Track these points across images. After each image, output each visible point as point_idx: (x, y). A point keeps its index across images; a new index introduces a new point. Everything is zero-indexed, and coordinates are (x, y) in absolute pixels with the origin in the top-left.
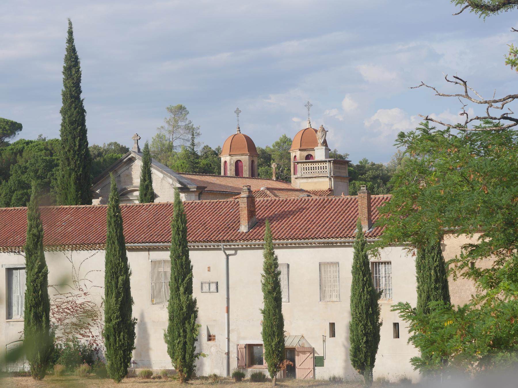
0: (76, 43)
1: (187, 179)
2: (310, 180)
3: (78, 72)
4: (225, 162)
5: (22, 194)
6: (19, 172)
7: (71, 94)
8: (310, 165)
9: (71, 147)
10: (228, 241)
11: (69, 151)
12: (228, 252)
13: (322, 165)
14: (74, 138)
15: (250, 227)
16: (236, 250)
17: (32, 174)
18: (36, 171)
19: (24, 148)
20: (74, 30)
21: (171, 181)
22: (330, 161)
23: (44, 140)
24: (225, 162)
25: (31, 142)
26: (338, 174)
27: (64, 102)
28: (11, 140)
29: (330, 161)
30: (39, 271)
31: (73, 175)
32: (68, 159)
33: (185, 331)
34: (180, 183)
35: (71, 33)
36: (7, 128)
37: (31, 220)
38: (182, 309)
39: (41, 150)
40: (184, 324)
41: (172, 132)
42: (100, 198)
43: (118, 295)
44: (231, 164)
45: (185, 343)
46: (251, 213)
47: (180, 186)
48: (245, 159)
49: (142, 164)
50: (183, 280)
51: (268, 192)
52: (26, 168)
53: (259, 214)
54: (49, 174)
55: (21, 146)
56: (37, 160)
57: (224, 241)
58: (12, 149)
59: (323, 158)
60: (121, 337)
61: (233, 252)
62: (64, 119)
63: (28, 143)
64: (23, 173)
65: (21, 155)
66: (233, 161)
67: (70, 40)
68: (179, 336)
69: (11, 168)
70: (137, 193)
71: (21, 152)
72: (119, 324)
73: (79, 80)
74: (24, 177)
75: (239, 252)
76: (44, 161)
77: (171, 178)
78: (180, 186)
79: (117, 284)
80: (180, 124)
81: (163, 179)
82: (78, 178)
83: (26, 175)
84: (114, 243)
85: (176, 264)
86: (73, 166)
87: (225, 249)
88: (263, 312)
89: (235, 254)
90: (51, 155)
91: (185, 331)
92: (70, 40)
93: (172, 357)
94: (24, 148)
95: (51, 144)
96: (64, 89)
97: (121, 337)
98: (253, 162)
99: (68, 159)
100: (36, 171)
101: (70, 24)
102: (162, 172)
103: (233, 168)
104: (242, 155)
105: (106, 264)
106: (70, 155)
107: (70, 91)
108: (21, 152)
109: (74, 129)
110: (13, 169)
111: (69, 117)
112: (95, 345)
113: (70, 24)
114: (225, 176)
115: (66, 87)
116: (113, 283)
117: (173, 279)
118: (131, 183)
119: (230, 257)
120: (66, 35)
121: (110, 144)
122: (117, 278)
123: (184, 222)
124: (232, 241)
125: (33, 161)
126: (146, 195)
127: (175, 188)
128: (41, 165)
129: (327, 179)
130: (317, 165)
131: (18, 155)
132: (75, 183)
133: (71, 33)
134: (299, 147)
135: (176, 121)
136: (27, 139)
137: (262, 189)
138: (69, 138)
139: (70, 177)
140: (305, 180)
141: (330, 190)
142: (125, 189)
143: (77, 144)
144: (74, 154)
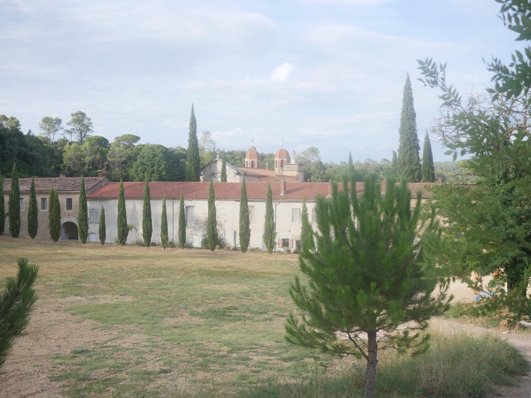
0: (195, 113)
1: (239, 170)
2: (289, 172)
3: (196, 125)
4: (247, 161)
5: (143, 168)
6: (141, 158)
7: (193, 134)
8: (289, 166)
9: (192, 155)
10: (276, 199)
11: (192, 157)
12: (276, 203)
13: (294, 166)
14: (194, 152)
15: (285, 194)
16: (279, 202)
17: (147, 159)
18: (148, 158)
19: (142, 147)
20: (194, 108)
21: (233, 170)
22: (297, 164)
23: (149, 144)
24: (247, 161)
25: (145, 145)
26: (300, 170)
27: (190, 137)
28: (135, 144)
29: (297, 164)
30: (214, 210)
31: (193, 167)
32: (191, 160)
33: (271, 235)
34: (237, 171)
35: (193, 109)
36: (135, 139)
37: (210, 191)
38: (270, 226)
39: (150, 149)
40: (271, 232)
41: (204, 143)
42: (203, 176)
43: (245, 220)
44: (250, 162)
45: (271, 239)
46: (285, 188)
47: (236, 172)
48: (256, 161)
49: (222, 163)
50: (271, 215)
51: (277, 177)
52: (144, 157)
53: (288, 189)
54: (154, 159)
55: (140, 147)
56: (148, 153)
57: (275, 199)
58: (137, 148)
59: (294, 163)
60: (246, 236)
61: (278, 203)
62: (190, 144)
63: (143, 146)
64: (143, 158)
65: (141, 151)
66: (251, 162)
67: (193, 112)
68: (269, 236)
69: (137, 156)
70: (220, 175)
71: (141, 149)
72: (245, 231)
73: (196, 128)
74: (143, 160)
75: (281, 203)
76: (152, 154)
77: (233, 169)
78: (236, 172)
79: (245, 216)
80: (207, 139)
81: (229, 169)
82: (195, 168)
83: (144, 160)
84: (244, 201)
85: (268, 209)
86: (193, 163)
87: (275, 202)
88: (302, 228)
89: (279, 204)
90: (154, 151)
91: (271, 235)
92: (193, 112)
93: (266, 244)
94: (142, 147)
95: (154, 146)
96: (190, 132)
97: (246, 236)
98: (258, 161)
99: (191, 160)
100: (148, 158)
101: (193, 105)
102: (229, 166)
103: (251, 164)
104: (255, 159)
105: (240, 209)
106: (192, 158)
107: (193, 132)
108: (141, 149)
109: (194, 148)
110: (138, 156)
111: (192, 143)
112: (221, 237)
113: (193, 105)
114: (247, 168)
115: (191, 131)
116: (243, 216)
117: (267, 215)
118: (217, 170)
119: (277, 205)
120: (191, 110)
121: (177, 147)
122: (245, 214)
123: (271, 194)
124: (278, 199)
125: (147, 153)
126: (223, 176)
127: (235, 173)
128: (151, 156)
129: (296, 172)
130: (292, 166)
131: (140, 151)
132: (194, 170)
133: (193, 109)
134: (278, 156)
135: (206, 138)
136: (143, 144)
137: (274, 176)
138: (192, 151)
139: (192, 167)
140: (287, 172)
141: (297, 176)
142: (214, 172)
143: (195, 154)
144: (194, 158)
